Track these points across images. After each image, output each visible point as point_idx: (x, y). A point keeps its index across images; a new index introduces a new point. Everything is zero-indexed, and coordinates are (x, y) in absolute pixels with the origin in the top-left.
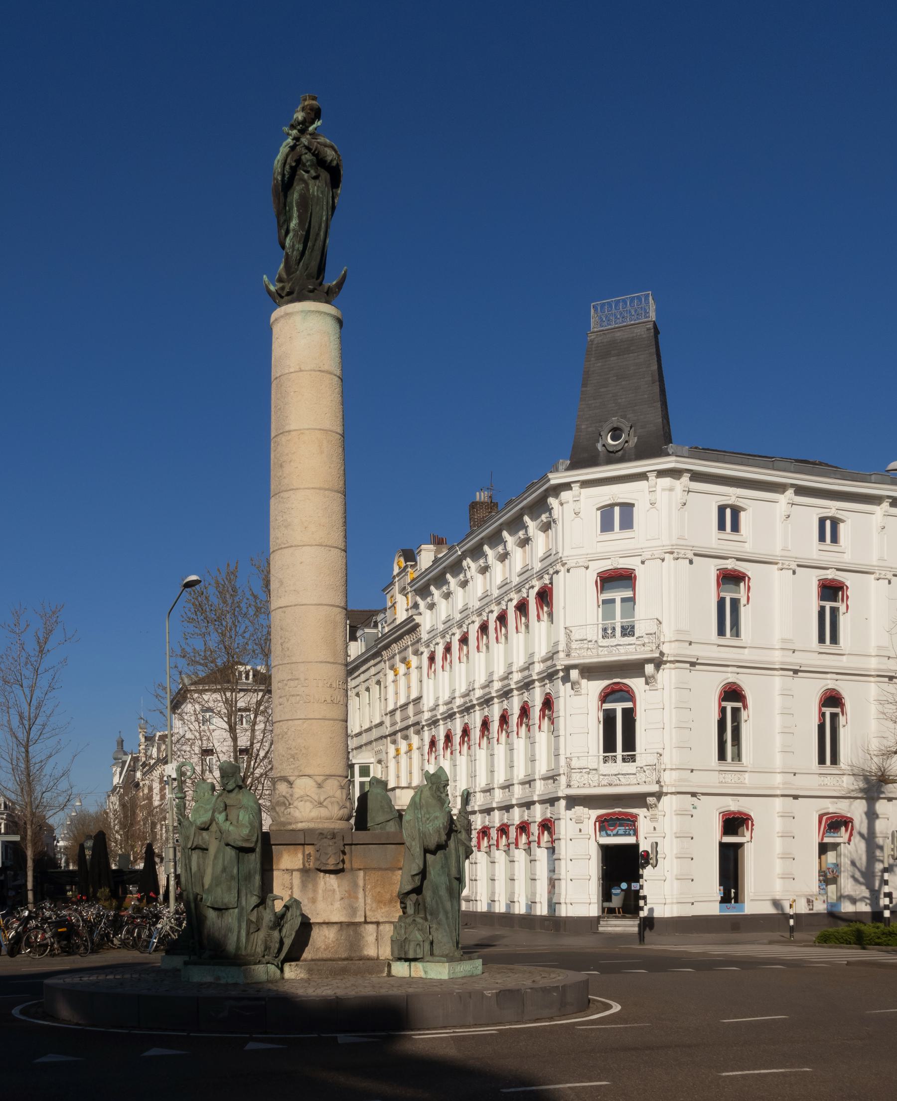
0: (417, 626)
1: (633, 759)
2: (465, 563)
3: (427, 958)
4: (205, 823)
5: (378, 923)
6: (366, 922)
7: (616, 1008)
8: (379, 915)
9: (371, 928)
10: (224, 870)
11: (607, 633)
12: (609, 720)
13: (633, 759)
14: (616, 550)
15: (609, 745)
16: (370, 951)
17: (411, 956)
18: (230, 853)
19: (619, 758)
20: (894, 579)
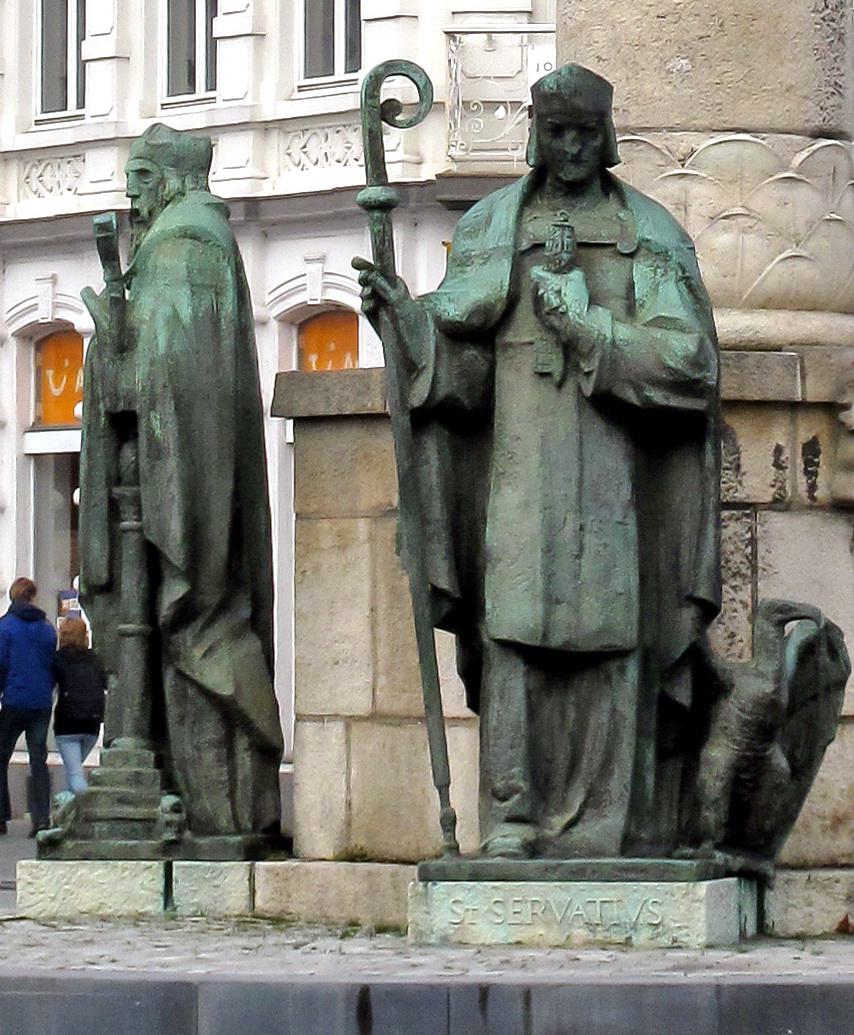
4: (482, 310)
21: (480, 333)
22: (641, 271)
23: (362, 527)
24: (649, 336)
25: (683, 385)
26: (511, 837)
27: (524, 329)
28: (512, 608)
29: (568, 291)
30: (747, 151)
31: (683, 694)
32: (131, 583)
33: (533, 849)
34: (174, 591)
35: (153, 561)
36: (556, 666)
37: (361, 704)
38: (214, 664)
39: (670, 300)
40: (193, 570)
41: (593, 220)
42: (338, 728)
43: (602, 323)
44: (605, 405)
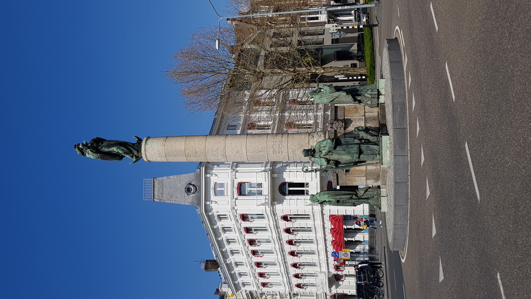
0: (250, 292)
1: (307, 184)
2: (228, 262)
3: (377, 88)
5: (365, 112)
6: (365, 116)
7: (397, 28)
8: (362, 113)
9: (366, 114)
10: (344, 150)
11: (260, 193)
12: (292, 193)
13: (307, 184)
14: (230, 190)
15: (302, 193)
16: (376, 114)
17: (376, 93)
18: (338, 148)
19: (307, 189)
20: (218, 296)
21: (328, 161)
22: (321, 146)
23: (347, 178)
24: (328, 144)
25: (333, 141)
26: (378, 156)
27: (327, 157)
28: (356, 159)
29: (324, 152)
30: (311, 140)
31: (363, 141)
32: (353, 201)
33: (379, 154)
34: (354, 197)
35: (351, 198)
36: (361, 152)
37: (365, 178)
38: (361, 193)
39: (325, 143)
40: (352, 194)
41: (317, 151)
42: (368, 181)
43: (327, 149)
44: (335, 148)
